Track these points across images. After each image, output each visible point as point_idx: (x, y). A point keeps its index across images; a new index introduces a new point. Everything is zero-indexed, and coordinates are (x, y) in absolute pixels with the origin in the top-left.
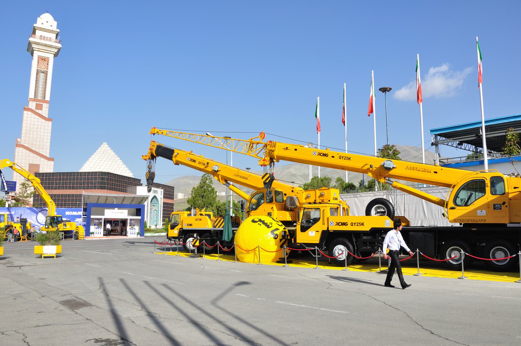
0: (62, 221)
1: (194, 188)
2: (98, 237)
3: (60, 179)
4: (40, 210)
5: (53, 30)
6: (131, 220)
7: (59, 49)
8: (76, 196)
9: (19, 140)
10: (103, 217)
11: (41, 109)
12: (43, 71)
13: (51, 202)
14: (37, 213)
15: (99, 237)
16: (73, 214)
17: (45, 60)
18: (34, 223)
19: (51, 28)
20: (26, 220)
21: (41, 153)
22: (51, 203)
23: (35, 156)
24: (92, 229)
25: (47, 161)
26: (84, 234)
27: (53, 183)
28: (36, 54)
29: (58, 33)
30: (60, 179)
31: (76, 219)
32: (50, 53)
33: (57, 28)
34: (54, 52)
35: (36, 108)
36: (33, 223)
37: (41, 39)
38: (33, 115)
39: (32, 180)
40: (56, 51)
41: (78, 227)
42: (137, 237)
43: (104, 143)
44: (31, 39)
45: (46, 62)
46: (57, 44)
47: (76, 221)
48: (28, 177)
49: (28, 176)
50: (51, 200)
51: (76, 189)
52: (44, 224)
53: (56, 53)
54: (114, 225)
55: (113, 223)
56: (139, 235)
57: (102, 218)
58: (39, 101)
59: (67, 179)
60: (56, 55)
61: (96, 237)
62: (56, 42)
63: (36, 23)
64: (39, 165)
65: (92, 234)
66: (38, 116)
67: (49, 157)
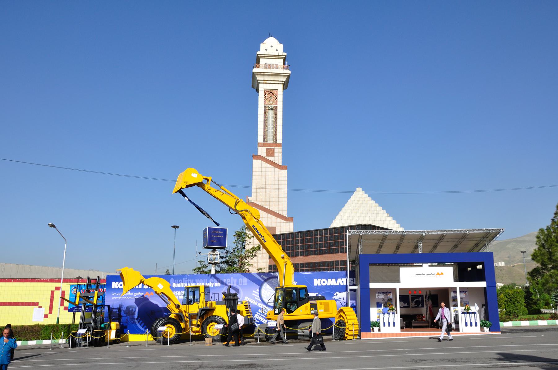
0: (308, 299)
1: (542, 230)
2: (389, 335)
3: (302, 241)
4: (266, 278)
5: (279, 55)
6: (463, 290)
7: (289, 77)
8: (327, 264)
9: (250, 198)
10: (396, 286)
11: (273, 155)
12: (272, 108)
13: (283, 258)
14: (261, 285)
15: (393, 335)
16: (329, 284)
17: (273, 93)
18: (256, 304)
19: (276, 53)
20: (235, 297)
21: (277, 212)
22: (283, 260)
23: (270, 216)
24: (374, 314)
25: (284, 221)
26: (357, 327)
27: (293, 248)
28: (262, 87)
29: (285, 58)
30: (302, 241)
31: (335, 294)
32: (278, 84)
33: (284, 52)
34: (283, 81)
35: (267, 155)
36: (254, 303)
37: (266, 68)
38: (264, 164)
39: (244, 212)
40: (285, 80)
41: (342, 311)
42: (483, 333)
43: (357, 189)
44: (255, 70)
45: (273, 97)
46: (285, 70)
47: (334, 299)
48: (235, 207)
49: (236, 204)
50: (283, 254)
51: (325, 253)
52: (272, 304)
53: (285, 82)
54: (413, 305)
55: (412, 300)
56: (487, 327)
57: (395, 289)
58: (270, 145)
59: (311, 240)
60: (285, 86)
61: (385, 335)
62: (284, 68)
63: (259, 50)
64: (275, 228)
65: (375, 326)
66: (270, 164)
67: (286, 216)
